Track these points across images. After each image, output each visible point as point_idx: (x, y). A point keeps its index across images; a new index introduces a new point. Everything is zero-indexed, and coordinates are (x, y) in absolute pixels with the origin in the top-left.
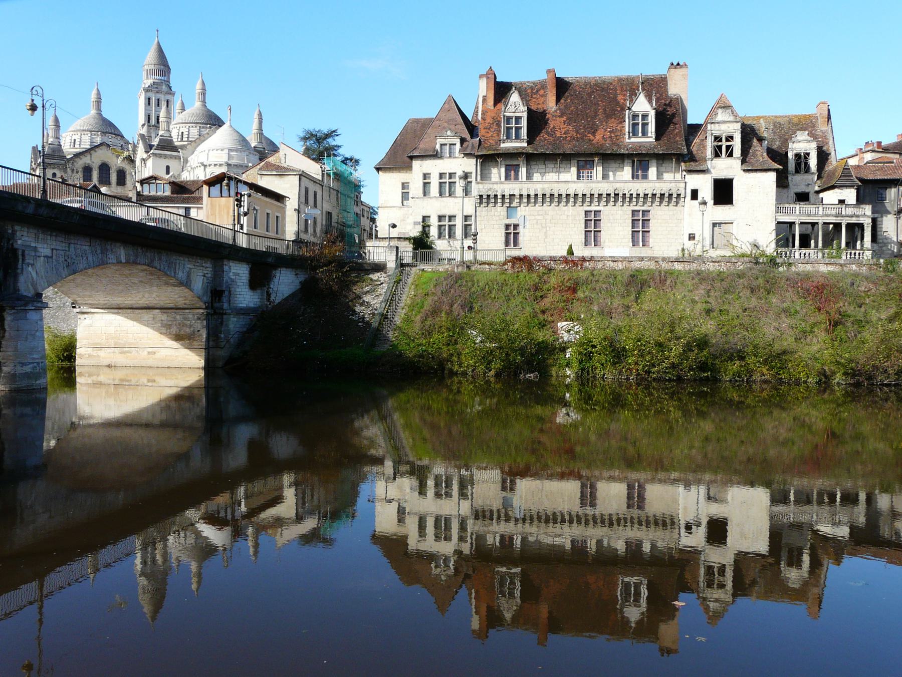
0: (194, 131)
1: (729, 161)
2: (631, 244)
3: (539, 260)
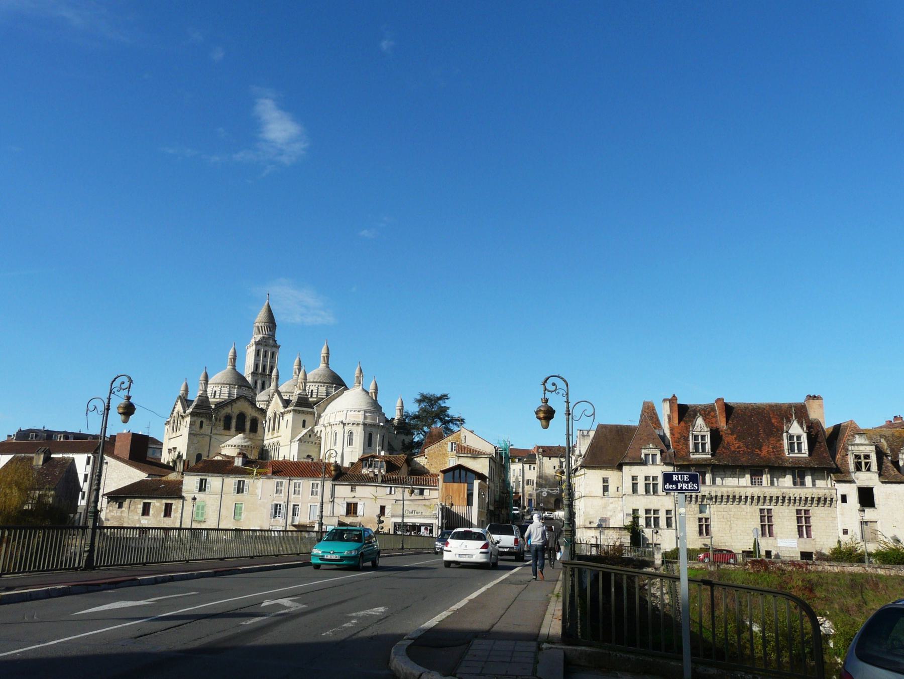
0: (323, 390)
1: (868, 474)
2: (798, 536)
3: (773, 563)
